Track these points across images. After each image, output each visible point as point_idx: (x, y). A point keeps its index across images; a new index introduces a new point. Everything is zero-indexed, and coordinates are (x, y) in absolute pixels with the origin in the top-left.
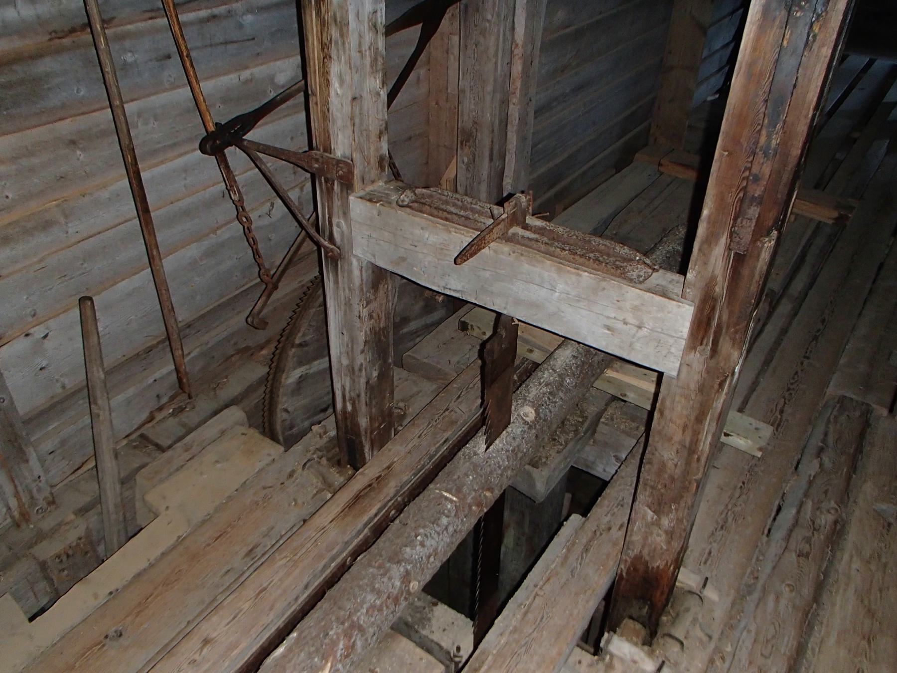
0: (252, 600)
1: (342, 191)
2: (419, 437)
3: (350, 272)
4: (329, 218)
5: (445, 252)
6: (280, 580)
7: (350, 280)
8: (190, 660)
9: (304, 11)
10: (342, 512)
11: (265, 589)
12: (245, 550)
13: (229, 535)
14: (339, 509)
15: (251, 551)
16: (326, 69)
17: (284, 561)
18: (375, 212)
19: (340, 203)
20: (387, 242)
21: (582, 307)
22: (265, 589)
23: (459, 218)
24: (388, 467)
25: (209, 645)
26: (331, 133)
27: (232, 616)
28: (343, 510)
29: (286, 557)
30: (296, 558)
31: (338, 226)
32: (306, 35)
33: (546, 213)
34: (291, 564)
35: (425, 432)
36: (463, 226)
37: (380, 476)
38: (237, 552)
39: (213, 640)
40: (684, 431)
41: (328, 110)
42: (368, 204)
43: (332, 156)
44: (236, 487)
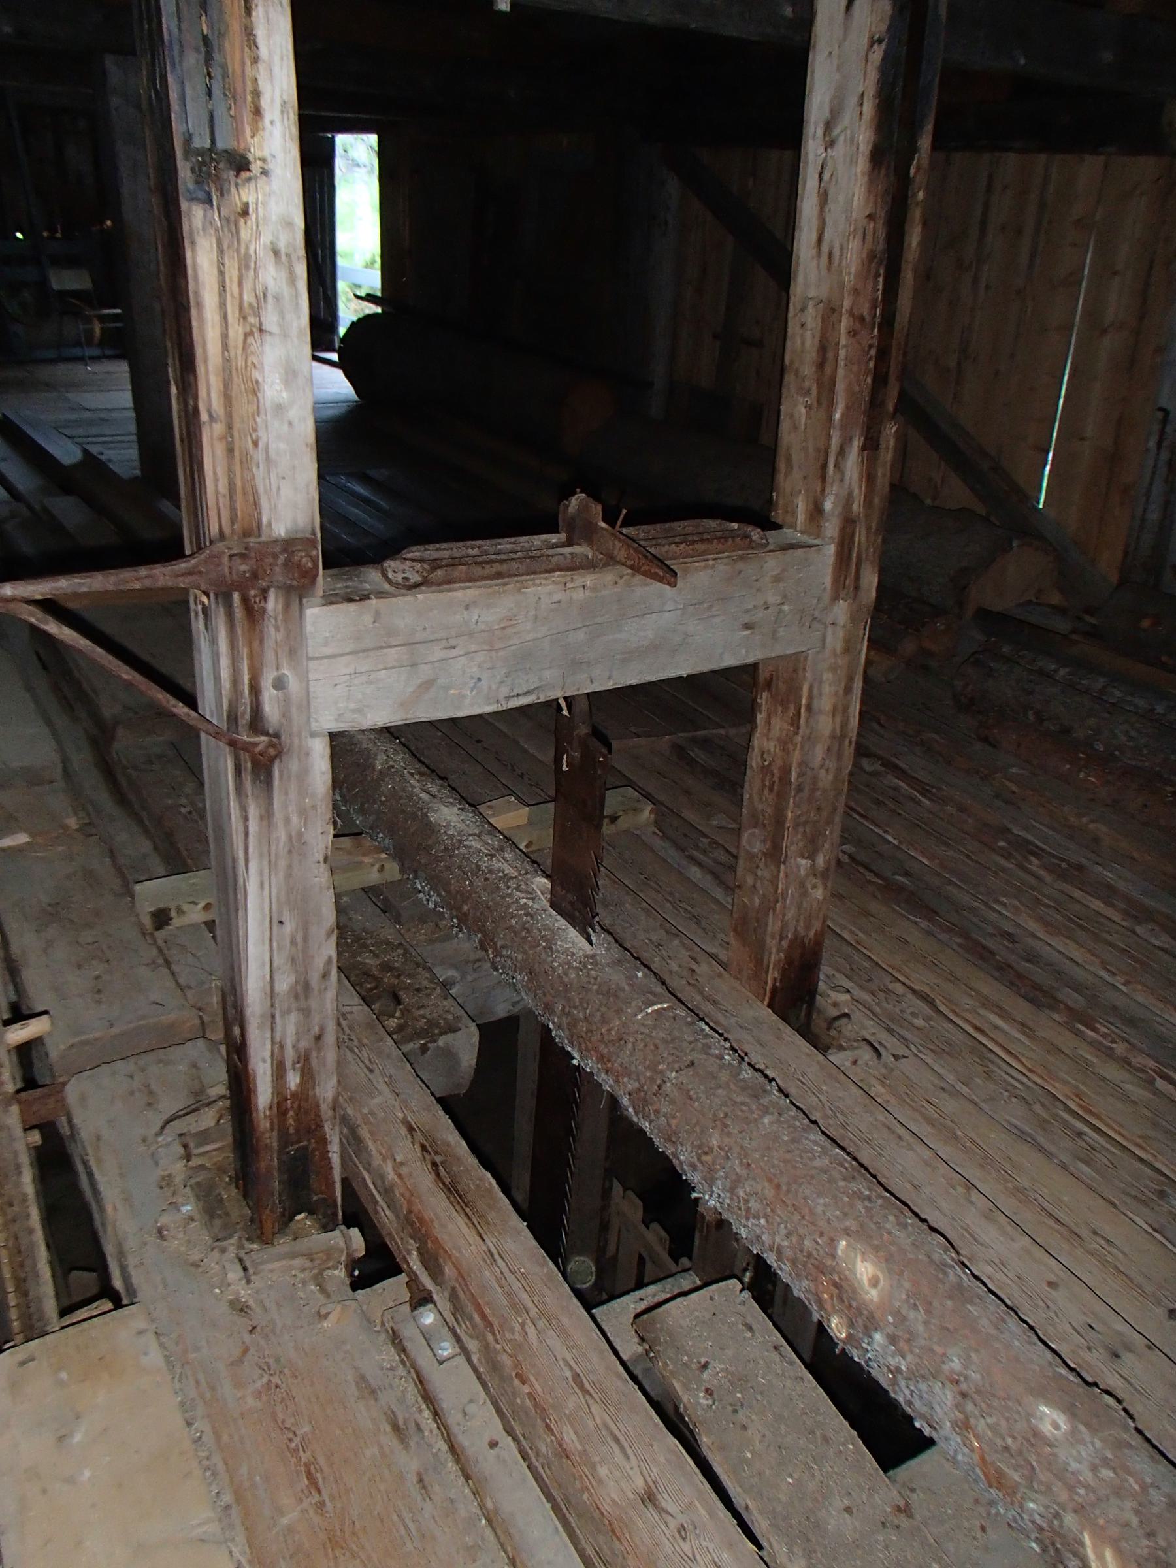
0: (590, 1402)
1: (287, 606)
2: (371, 1071)
3: (305, 772)
4: (251, 680)
5: (510, 631)
6: (569, 1348)
7: (303, 791)
8: (677, 1536)
9: (193, 243)
10: (469, 1218)
11: (576, 1377)
12: (389, 1440)
13: (322, 1461)
14: (461, 1221)
15: (396, 1428)
16: (251, 359)
17: (531, 1330)
18: (368, 619)
19: (280, 636)
20: (394, 667)
21: (715, 613)
22: (576, 1377)
23: (521, 563)
24: (411, 1129)
25: (659, 1497)
26: (261, 490)
27: (614, 1445)
28: (467, 1215)
29: (523, 1325)
30: (534, 1312)
31: (279, 684)
32: (196, 293)
33: (620, 512)
34: (541, 1324)
35: (367, 1062)
36: (528, 574)
37: (423, 1147)
38: (383, 1455)
39: (649, 1487)
40: (834, 716)
41: (256, 443)
42: (352, 607)
43: (263, 538)
44: (181, 1423)
